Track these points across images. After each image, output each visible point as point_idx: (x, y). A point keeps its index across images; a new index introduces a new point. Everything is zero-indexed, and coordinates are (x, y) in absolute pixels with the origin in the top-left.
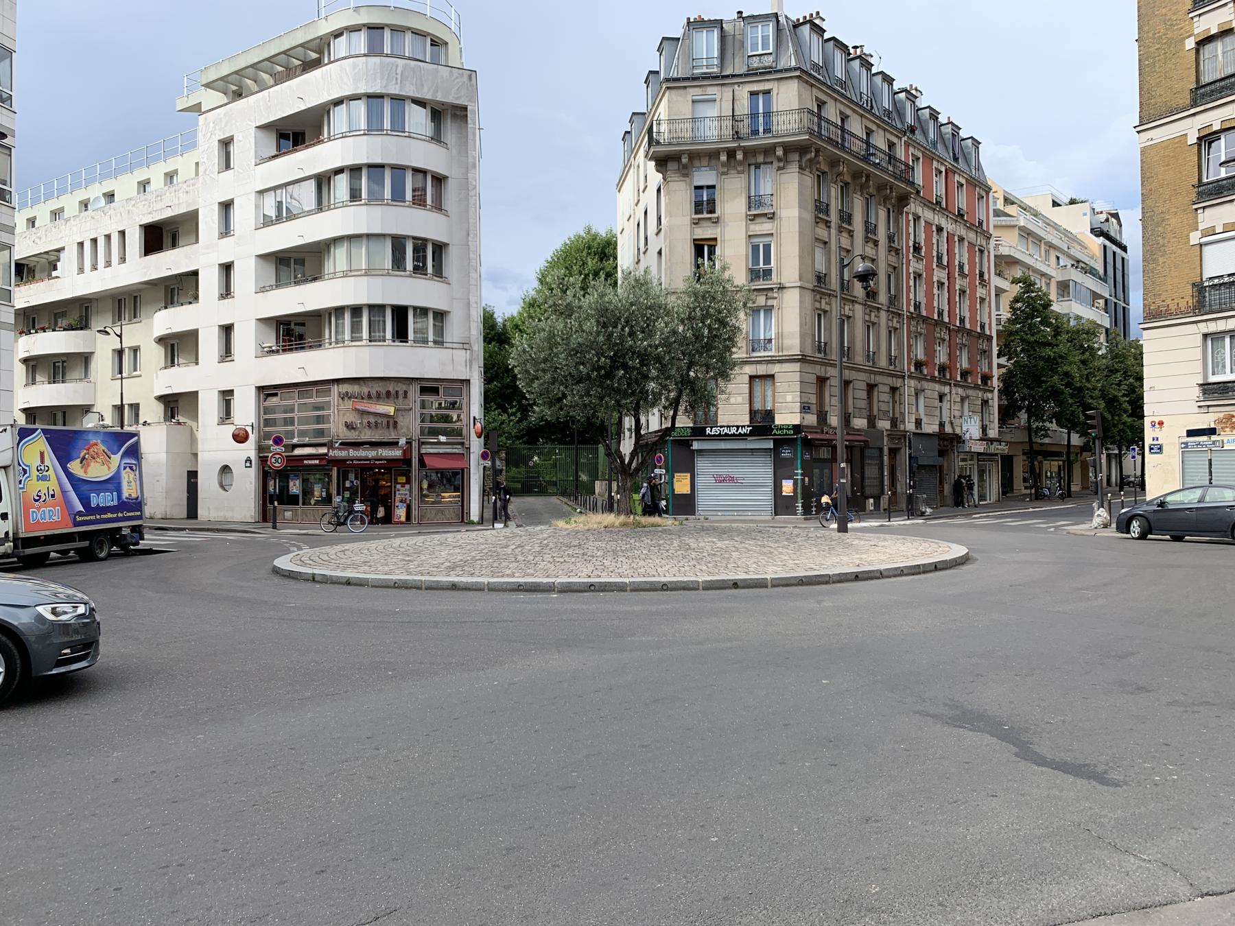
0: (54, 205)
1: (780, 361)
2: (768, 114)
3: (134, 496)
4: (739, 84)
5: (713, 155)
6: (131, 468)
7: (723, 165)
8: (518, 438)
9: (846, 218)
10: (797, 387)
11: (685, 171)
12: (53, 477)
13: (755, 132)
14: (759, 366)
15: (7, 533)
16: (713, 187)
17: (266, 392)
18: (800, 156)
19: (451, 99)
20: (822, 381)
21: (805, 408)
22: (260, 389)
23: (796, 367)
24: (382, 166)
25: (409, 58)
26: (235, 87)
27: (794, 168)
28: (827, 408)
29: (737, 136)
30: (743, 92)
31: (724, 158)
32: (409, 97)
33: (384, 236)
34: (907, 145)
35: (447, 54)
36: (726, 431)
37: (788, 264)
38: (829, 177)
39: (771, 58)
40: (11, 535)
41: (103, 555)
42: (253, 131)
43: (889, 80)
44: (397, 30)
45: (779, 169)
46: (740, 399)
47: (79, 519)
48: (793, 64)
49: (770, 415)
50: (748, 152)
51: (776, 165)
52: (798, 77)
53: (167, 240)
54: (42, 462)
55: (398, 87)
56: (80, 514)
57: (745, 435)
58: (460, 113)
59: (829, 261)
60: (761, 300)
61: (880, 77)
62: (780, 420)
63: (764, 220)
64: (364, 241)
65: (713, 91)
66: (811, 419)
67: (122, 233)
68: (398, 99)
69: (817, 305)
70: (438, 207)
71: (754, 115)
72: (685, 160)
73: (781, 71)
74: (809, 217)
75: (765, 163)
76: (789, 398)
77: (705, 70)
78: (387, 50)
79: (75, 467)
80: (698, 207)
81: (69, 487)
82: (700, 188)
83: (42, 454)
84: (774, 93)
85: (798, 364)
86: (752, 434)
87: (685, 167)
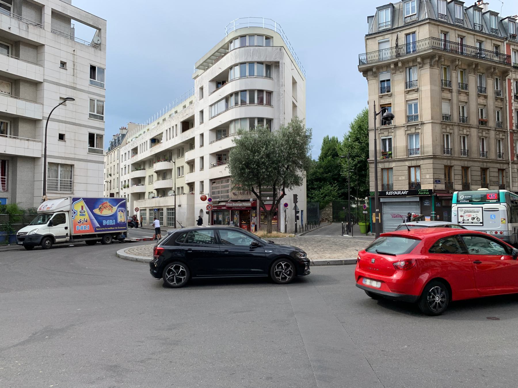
0: (163, 118)
1: (423, 159)
2: (414, 43)
3: (123, 221)
4: (400, 31)
5: (388, 66)
6: (122, 211)
7: (393, 69)
8: (339, 197)
9: (464, 87)
10: (431, 171)
11: (375, 75)
12: (86, 213)
13: (408, 53)
14: (413, 162)
15: (67, 234)
16: (389, 80)
17: (213, 181)
18: (431, 60)
19: (272, 59)
20: (448, 169)
21: (436, 181)
22: (211, 180)
23: (431, 161)
24: (245, 91)
25: (256, 46)
26: (205, 66)
27: (427, 66)
28: (453, 181)
29: (398, 55)
30: (402, 35)
31: (392, 66)
32: (255, 62)
33: (245, 119)
34: (508, 45)
35: (273, 41)
36: (396, 193)
37: (426, 112)
38: (451, 68)
39: (416, 16)
40: (69, 234)
41: (109, 242)
42: (208, 83)
43: (496, 14)
44: (251, 35)
45: (420, 68)
46: (404, 178)
47: (97, 229)
48: (427, 17)
49: (418, 185)
50: (404, 62)
51: (418, 66)
52: (428, 23)
53: (190, 125)
54: (82, 209)
55: (251, 58)
56: (98, 227)
57: (405, 195)
58: (277, 64)
59: (452, 109)
60: (413, 130)
61: (488, 14)
62: (423, 187)
63: (413, 92)
64: (239, 121)
65: (388, 37)
66: (441, 187)
67: (176, 125)
68: (251, 63)
69: (444, 130)
70: (269, 103)
71: (407, 44)
72: (374, 70)
73: (420, 21)
74: (437, 88)
75: (414, 66)
76: (428, 176)
77: (385, 28)
78: (247, 44)
79: (97, 211)
80: (382, 90)
81: (93, 218)
82: (384, 81)
83: (82, 207)
84: (417, 33)
85: (432, 160)
86: (408, 194)
87: (375, 73)
